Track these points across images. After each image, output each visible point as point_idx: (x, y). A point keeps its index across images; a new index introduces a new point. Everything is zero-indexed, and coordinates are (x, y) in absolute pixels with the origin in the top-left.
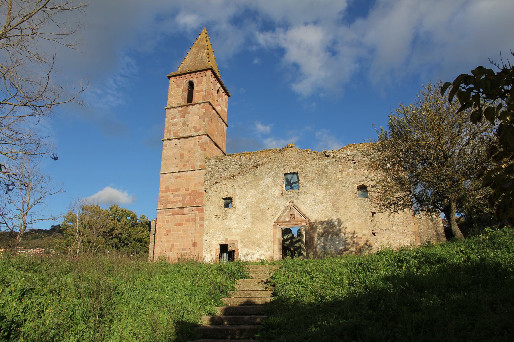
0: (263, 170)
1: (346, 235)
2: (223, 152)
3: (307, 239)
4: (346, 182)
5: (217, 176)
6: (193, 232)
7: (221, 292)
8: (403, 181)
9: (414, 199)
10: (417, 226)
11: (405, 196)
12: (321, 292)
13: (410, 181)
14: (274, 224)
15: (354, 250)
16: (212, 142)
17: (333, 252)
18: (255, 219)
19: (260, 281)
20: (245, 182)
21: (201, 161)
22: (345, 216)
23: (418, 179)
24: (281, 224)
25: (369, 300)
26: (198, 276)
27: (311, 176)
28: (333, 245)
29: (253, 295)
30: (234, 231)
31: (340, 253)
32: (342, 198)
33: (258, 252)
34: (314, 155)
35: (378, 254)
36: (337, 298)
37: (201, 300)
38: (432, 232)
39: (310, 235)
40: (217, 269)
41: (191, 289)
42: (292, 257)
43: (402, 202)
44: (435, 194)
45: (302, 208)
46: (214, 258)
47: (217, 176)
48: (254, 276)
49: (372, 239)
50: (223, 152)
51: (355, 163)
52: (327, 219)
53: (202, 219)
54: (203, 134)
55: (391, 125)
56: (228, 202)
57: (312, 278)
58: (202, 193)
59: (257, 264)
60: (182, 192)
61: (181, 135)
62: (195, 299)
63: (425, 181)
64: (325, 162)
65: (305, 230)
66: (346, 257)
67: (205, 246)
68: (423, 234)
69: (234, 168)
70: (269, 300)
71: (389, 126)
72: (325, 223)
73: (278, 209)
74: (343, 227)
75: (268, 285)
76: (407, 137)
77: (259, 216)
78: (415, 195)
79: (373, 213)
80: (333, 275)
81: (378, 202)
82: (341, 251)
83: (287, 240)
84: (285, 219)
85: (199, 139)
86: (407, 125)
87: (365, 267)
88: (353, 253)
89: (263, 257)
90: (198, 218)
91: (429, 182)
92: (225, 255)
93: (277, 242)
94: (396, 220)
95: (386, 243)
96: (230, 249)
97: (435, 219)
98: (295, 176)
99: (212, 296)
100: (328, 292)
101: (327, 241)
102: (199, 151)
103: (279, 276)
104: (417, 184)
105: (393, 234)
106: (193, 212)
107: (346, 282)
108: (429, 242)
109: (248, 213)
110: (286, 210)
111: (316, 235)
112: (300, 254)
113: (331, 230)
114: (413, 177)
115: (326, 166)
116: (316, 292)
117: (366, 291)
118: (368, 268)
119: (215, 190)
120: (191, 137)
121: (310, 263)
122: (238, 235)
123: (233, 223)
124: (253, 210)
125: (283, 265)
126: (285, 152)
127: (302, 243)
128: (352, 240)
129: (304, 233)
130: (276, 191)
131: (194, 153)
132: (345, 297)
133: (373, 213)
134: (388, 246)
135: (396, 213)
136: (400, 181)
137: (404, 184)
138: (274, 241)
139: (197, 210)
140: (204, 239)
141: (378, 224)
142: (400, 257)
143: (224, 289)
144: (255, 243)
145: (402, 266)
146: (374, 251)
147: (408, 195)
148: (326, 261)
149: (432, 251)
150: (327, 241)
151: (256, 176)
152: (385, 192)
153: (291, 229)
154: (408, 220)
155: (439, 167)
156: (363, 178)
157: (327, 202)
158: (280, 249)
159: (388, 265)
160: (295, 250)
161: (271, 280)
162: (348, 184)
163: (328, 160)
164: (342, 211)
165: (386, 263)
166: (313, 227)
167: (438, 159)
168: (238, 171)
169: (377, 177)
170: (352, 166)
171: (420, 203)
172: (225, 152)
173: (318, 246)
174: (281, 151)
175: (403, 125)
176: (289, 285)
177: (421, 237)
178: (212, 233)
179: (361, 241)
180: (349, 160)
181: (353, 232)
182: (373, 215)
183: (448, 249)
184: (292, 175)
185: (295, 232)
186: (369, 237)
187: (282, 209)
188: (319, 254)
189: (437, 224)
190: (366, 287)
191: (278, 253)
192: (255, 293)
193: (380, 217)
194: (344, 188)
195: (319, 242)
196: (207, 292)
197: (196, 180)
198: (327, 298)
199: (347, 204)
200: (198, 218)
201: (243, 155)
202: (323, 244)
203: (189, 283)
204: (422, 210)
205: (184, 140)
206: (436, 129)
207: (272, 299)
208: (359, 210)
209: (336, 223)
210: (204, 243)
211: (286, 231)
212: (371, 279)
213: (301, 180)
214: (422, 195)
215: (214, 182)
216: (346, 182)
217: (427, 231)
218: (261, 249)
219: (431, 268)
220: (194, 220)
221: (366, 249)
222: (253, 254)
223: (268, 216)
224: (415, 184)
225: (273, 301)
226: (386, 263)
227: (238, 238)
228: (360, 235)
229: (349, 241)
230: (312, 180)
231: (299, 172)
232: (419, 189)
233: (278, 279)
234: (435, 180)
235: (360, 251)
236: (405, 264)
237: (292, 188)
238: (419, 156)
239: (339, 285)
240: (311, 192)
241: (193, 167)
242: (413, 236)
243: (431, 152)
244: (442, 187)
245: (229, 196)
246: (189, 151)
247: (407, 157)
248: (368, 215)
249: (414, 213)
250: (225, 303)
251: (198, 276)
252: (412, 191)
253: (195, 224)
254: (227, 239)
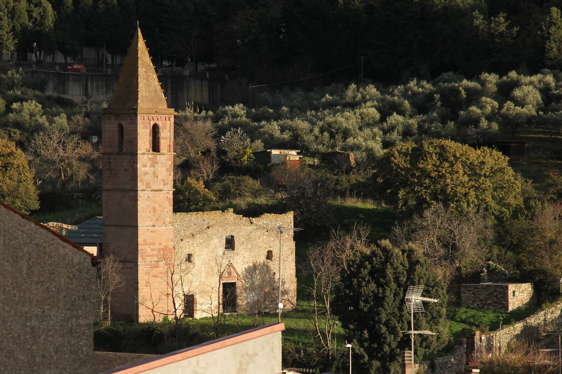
56: (189, 258)
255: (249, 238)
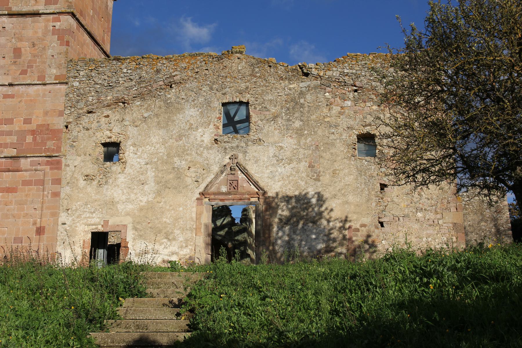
0: (183, 94)
1: (331, 224)
2: (105, 53)
3: (259, 227)
4: (336, 126)
5: (90, 99)
6: (38, 206)
7: (91, 321)
8: (443, 128)
9: (460, 164)
10: (461, 214)
11: (444, 157)
12: (279, 324)
13: (456, 130)
14: (198, 196)
15: (344, 250)
16: (81, 30)
17: (305, 254)
18: (163, 186)
19: (167, 302)
20: (146, 115)
21: (59, 67)
22: (331, 189)
23: (470, 127)
24: (212, 197)
25: (366, 341)
26: (45, 290)
27: (273, 110)
28: (306, 241)
29: (151, 328)
30: (120, 207)
31: (318, 255)
32: (327, 155)
33: (165, 248)
34: (281, 70)
35: (387, 260)
36: (307, 336)
37: (49, 338)
38: (488, 227)
39: (264, 220)
40: (84, 279)
41: (30, 316)
42: (229, 261)
43: (437, 168)
44: (501, 156)
45: (252, 169)
46: (79, 258)
47: (90, 99)
48: (155, 291)
49: (377, 234)
50: (105, 53)
51: (356, 91)
52: (297, 193)
53: (57, 181)
54: (63, 10)
55: (431, 21)
56: (112, 151)
57: (263, 299)
58: (59, 131)
59: (163, 270)
60: (18, 125)
61: (15, 9)
62: (36, 335)
63: (484, 132)
64: (301, 85)
65: (256, 211)
66: (329, 264)
67: (61, 234)
68: (472, 229)
69: (126, 85)
70: (181, 337)
71: (427, 23)
72: (294, 200)
73: (206, 168)
74: (326, 209)
75: (182, 310)
76: (458, 46)
77: (170, 180)
78: (462, 156)
79: (383, 186)
80: (302, 294)
81: (393, 167)
82: (319, 251)
83: (222, 227)
84: (219, 188)
85: (55, 20)
86: (462, 22)
87: (361, 281)
88: (342, 257)
89: (174, 258)
90: (49, 178)
91: (491, 133)
92: (101, 253)
93: (202, 230)
94: (423, 200)
95: (402, 241)
96: (112, 240)
97: (496, 202)
98: (243, 109)
99: (72, 329)
100: (291, 325)
101: (294, 232)
102: (54, 46)
103: (203, 294)
104: (467, 136)
105: (416, 226)
106: (39, 167)
107: (326, 307)
108: (481, 245)
109: (151, 174)
110: (222, 172)
111: (276, 220)
112: (244, 255)
113: (304, 212)
114: (462, 123)
115: (302, 94)
116: (271, 324)
117: (362, 324)
118: (366, 284)
119: (87, 126)
121: (262, 272)
122: (128, 214)
123: (120, 192)
124: (160, 168)
125: (211, 272)
126: (226, 62)
127: (250, 234)
128: (341, 232)
129: (253, 216)
130: (206, 135)
131: (44, 49)
132: (322, 334)
133: (383, 186)
134: (405, 247)
135: (424, 188)
136: (437, 129)
137: (444, 135)
138: (197, 229)
139: (48, 163)
140: (61, 220)
141: (390, 205)
142: (426, 268)
143: (96, 315)
144: (160, 232)
145: (428, 283)
146: (379, 256)
147: (450, 156)
148: (290, 269)
149: (486, 259)
150: (294, 232)
151: (168, 105)
152: (407, 149)
153: (231, 208)
154: (445, 201)
155: (513, 107)
156: (370, 119)
157: (299, 161)
158: (207, 244)
159: (404, 281)
160: (235, 247)
161: (188, 300)
162: (340, 130)
163: (306, 83)
164: (326, 178)
165: (400, 276)
166: (270, 205)
167: (512, 90)
168: (134, 91)
169: (396, 120)
170: (351, 95)
171: (470, 172)
172: (108, 52)
173: (279, 242)
174: (219, 59)
175: (454, 21)
176: (220, 309)
177: (467, 235)
178: (76, 210)
179: (356, 236)
180: (346, 84)
181: (344, 218)
182: (382, 189)
183: (515, 257)
184: (236, 106)
185: (237, 214)
186: (373, 229)
187: (216, 169)
188: (279, 255)
189: (499, 211)
190: (362, 318)
191: (203, 251)
192: (157, 323)
193: (394, 194)
194: (332, 137)
195: (280, 234)
196: (62, 321)
197: (46, 103)
198: (290, 335)
199: (336, 166)
200: (49, 178)
201: (145, 62)
202: (287, 238)
203: (25, 304)
204: (473, 185)
205: (21, 19)
206: (516, 34)
207: (188, 334)
208: (356, 179)
209: (314, 201)
210: (61, 228)
211: (220, 212)
212: (371, 303)
213: (254, 118)
214: (476, 157)
215: (85, 110)
216: (336, 126)
217: (479, 223)
218: (171, 239)
219: (481, 290)
220: (42, 183)
221: (366, 251)
222: (156, 252)
223: (189, 180)
224: (465, 137)
225: (190, 338)
226: (400, 276)
227: (128, 221)
228: (355, 225)
229: (335, 234)
230: (275, 118)
231: (252, 100)
232: (471, 146)
233: (201, 298)
234: (503, 131)
235: (354, 253)
236: (434, 280)
237: (236, 131)
238: (478, 83)
239: (312, 312)
240: (271, 140)
241: (41, 77)
242: (453, 232)
243: (502, 78)
244: (514, 144)
245: (114, 139)
246: (34, 45)
247: (455, 84)
248: (373, 189)
249: (459, 190)
250: (97, 342)
251: (45, 290)
252: (459, 149)
253: (43, 190)
254: (106, 222)
255: (294, 104)
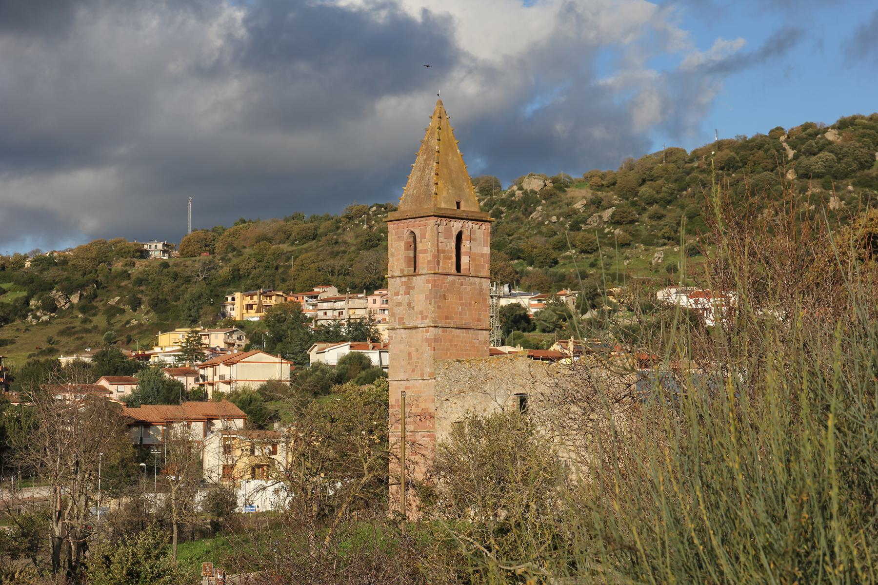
120: (416, 328)
